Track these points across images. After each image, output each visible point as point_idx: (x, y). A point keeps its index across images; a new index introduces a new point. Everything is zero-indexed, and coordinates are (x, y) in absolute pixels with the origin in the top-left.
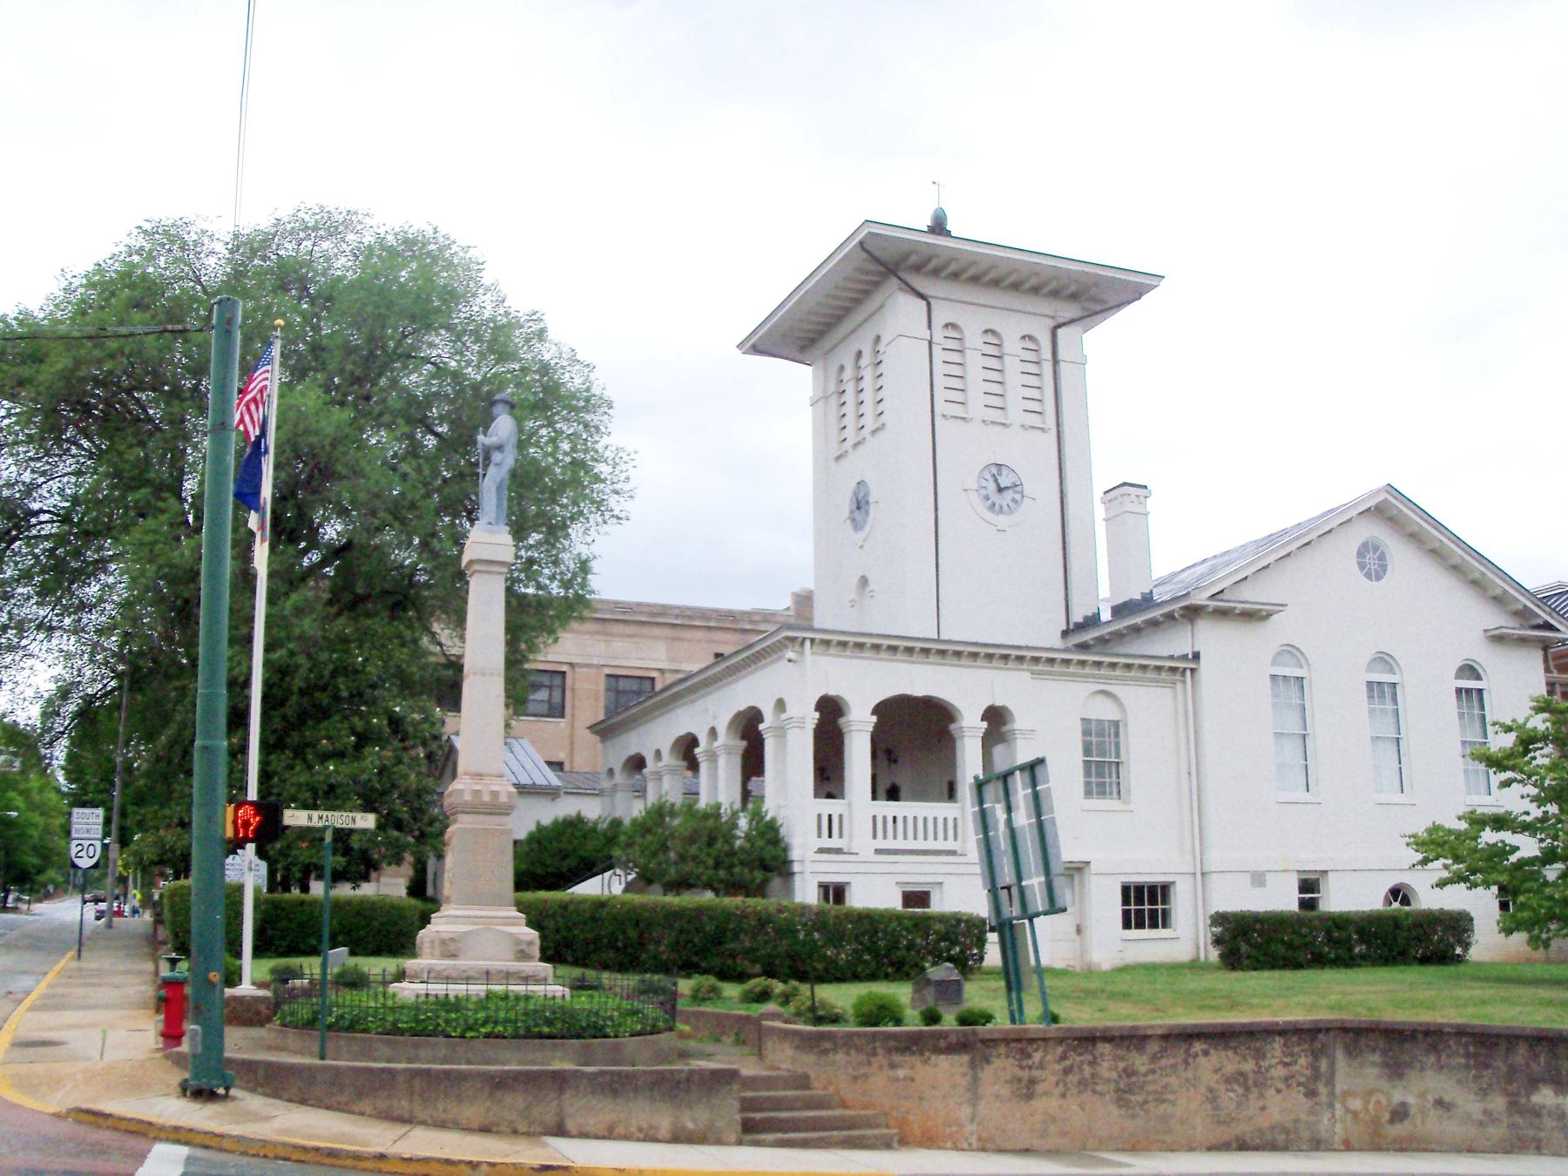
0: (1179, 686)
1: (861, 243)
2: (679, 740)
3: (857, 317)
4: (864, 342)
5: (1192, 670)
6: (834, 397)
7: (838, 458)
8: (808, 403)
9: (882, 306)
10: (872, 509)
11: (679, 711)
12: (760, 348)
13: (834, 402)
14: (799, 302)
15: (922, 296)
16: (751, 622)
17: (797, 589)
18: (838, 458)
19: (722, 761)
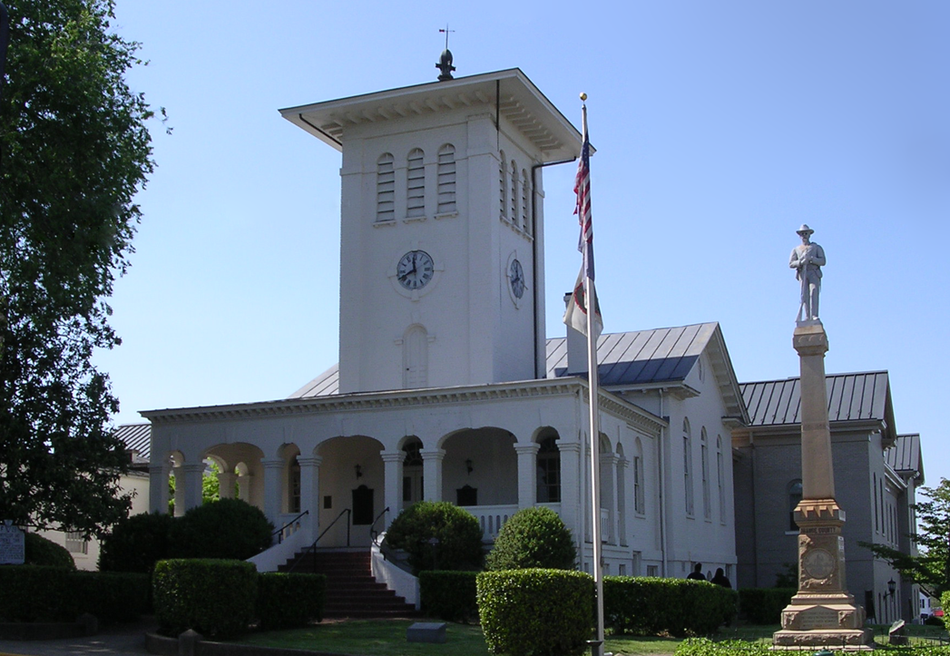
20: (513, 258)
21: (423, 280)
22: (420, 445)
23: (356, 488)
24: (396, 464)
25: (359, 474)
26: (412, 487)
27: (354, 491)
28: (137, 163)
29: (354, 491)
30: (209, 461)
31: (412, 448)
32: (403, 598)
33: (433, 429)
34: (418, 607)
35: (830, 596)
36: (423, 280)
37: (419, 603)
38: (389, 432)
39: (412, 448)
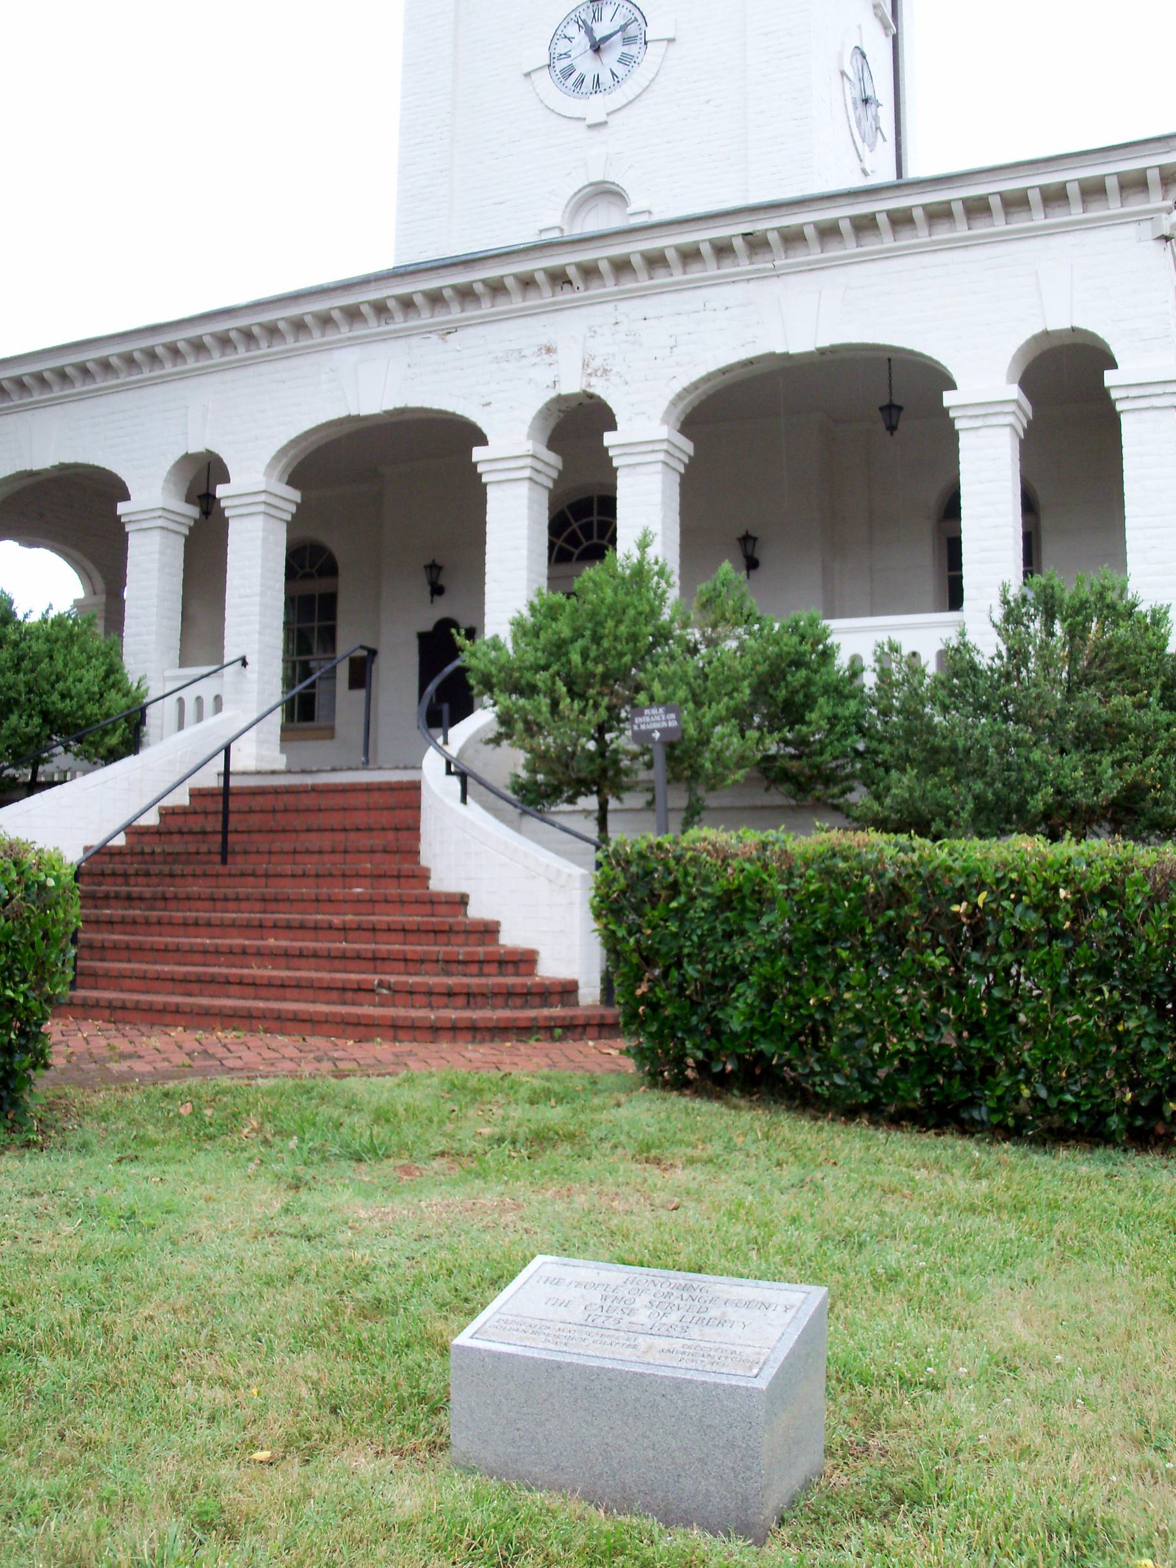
20: (849, 50)
21: (620, 70)
22: (608, 421)
23: (428, 626)
24: (524, 489)
25: (437, 590)
26: (581, 524)
27: (423, 637)
28: (540, 777)
29: (423, 637)
30: (1168, 1114)
31: (578, 426)
32: (462, 901)
33: (651, 362)
34: (590, 993)
35: (205, 1001)
36: (620, 70)
37: (541, 985)
38: (492, 387)
39: (578, 426)
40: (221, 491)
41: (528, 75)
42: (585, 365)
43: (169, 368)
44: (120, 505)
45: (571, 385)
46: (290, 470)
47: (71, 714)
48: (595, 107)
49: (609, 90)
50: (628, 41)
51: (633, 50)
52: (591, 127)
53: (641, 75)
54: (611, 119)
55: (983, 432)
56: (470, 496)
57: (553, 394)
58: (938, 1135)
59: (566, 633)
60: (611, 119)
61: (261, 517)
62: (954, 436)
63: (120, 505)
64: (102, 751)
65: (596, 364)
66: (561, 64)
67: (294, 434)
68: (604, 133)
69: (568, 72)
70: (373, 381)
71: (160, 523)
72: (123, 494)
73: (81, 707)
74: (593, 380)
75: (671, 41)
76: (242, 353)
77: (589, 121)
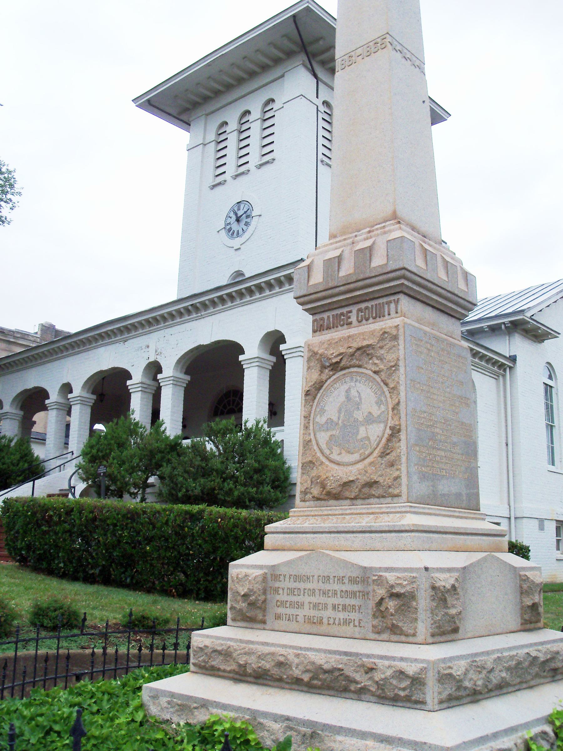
0: (501, 378)
1: (294, 16)
2: (269, 335)
3: (229, 97)
4: (255, 106)
5: (511, 368)
6: (236, 133)
7: (214, 187)
8: (185, 148)
9: (283, 76)
10: (254, 222)
11: (102, 350)
12: (152, 103)
13: (212, 147)
14: (208, 65)
15: (315, 76)
16: (15, 337)
17: (43, 322)
18: (214, 187)
19: (76, 410)
40: (282, 347)
41: (218, 232)
42: (156, 351)
43: (187, 317)
44: (128, 381)
45: (152, 359)
46: (187, 364)
47: (5, 469)
48: (236, 243)
49: (241, 236)
50: (248, 217)
51: (248, 220)
52: (236, 250)
53: (251, 229)
54: (242, 247)
55: (250, 369)
56: (238, 372)
57: (148, 362)
58: (18, 568)
59: (94, 443)
60: (242, 247)
61: (171, 385)
62: (243, 371)
63: (128, 381)
64: (16, 481)
65: (159, 351)
66: (228, 227)
67: (183, 353)
68: (239, 252)
69: (230, 230)
70: (105, 358)
71: (55, 407)
72: (241, 351)
73: (9, 467)
74: (158, 356)
75: (260, 216)
76: (258, 296)
77: (235, 248)
